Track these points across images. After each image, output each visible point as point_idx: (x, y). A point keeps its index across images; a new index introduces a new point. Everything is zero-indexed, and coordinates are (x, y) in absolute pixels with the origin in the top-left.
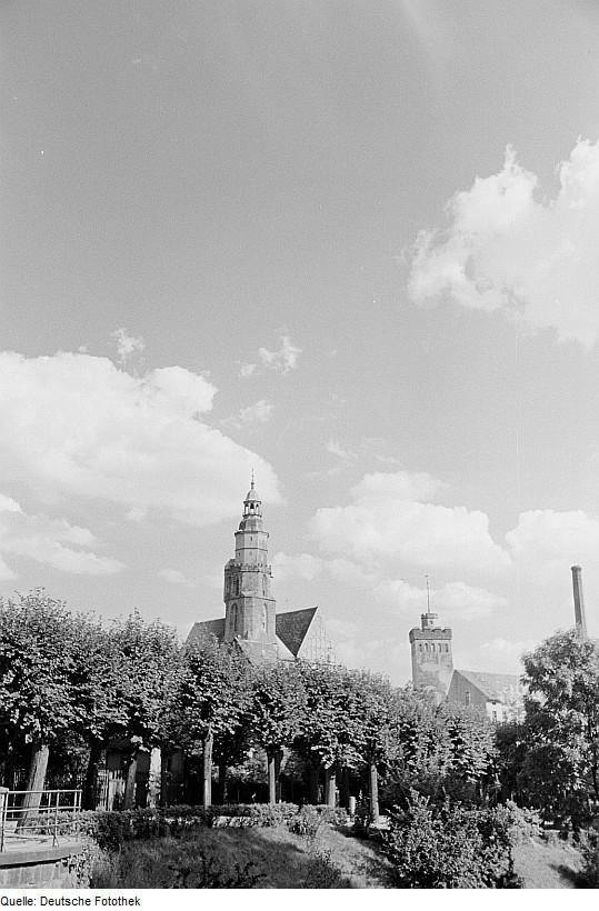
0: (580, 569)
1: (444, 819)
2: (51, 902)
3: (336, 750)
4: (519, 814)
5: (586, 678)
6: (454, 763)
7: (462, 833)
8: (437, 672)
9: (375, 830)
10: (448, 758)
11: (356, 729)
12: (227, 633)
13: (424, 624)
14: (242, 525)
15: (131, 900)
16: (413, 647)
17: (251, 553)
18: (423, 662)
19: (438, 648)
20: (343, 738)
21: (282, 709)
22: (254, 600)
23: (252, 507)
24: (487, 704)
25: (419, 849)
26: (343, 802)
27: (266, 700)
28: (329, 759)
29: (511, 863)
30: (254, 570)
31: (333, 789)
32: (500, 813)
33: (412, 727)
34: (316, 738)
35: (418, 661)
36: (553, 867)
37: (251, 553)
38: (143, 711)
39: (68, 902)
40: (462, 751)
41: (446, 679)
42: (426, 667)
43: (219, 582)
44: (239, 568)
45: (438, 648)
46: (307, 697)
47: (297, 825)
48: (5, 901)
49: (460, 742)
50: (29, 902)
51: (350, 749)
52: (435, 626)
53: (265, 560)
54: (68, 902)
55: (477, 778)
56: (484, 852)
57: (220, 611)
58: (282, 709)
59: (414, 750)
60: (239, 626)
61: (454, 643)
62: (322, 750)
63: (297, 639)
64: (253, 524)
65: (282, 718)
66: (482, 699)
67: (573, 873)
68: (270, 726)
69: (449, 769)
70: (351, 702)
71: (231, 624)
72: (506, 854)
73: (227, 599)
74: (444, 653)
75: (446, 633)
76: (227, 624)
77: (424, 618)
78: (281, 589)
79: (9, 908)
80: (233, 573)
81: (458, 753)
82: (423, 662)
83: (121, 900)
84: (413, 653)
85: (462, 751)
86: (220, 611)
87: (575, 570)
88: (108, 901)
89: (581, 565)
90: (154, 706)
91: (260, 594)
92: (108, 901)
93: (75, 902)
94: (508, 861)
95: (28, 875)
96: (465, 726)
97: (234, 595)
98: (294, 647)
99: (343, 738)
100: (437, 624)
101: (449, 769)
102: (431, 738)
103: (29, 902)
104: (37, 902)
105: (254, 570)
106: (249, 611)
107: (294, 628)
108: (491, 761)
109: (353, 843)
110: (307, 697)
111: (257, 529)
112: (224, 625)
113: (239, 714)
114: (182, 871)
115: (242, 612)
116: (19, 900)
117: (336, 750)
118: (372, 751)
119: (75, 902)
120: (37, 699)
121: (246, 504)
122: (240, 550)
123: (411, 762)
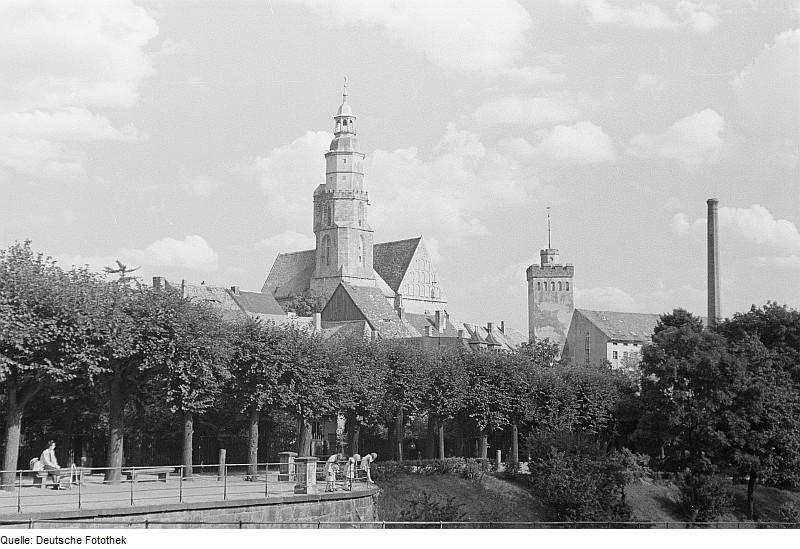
0: (717, 202)
1: (575, 468)
2: (46, 541)
3: (488, 417)
4: (633, 458)
5: (688, 366)
6: (579, 419)
7: (588, 476)
8: (556, 312)
9: (521, 475)
10: (574, 416)
11: (504, 399)
12: (318, 267)
13: (544, 260)
14: (334, 145)
15: (118, 539)
16: (531, 286)
17: (344, 178)
18: (540, 301)
20: (494, 407)
22: (349, 230)
23: (345, 123)
25: (557, 487)
26: (492, 455)
27: (438, 383)
29: (624, 496)
30: (348, 196)
31: (486, 446)
32: (615, 458)
34: (471, 409)
35: (536, 301)
36: (655, 498)
37: (344, 178)
38: (364, 398)
39: (61, 541)
40: (586, 409)
41: (565, 319)
42: (544, 307)
43: (305, 210)
46: (468, 378)
48: (4, 540)
49: (585, 401)
50: (26, 541)
51: (499, 416)
52: (556, 262)
54: (61, 541)
55: (597, 430)
56: (604, 489)
58: (451, 389)
59: (547, 412)
61: (575, 281)
63: (397, 273)
64: (346, 143)
65: (451, 396)
66: (603, 338)
67: (672, 503)
69: (575, 425)
72: (620, 490)
73: (318, 229)
74: (564, 291)
75: (568, 270)
76: (318, 256)
77: (544, 254)
79: (8, 546)
80: (324, 200)
81: (582, 411)
82: (540, 301)
83: (109, 540)
84: (530, 291)
85: (586, 409)
87: (711, 203)
88: (98, 541)
91: (356, 224)
92: (98, 541)
93: (68, 541)
94: (621, 495)
101: (575, 425)
103: (26, 541)
104: (34, 541)
105: (348, 196)
106: (342, 243)
107: (393, 259)
108: (611, 416)
110: (468, 378)
111: (351, 149)
114: (412, 502)
115: (336, 245)
116: (17, 540)
117: (488, 417)
118: (516, 416)
119: (68, 541)
120: (311, 397)
121: (338, 120)
122: (331, 174)
123: (544, 421)
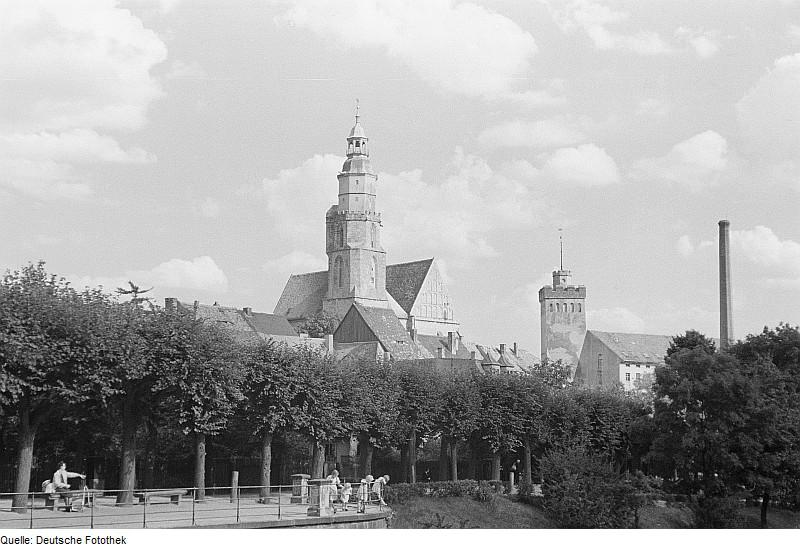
0: (728, 224)
2: (46, 541)
13: (556, 282)
14: (347, 166)
15: (118, 539)
16: (543, 307)
17: (357, 199)
18: (553, 323)
19: (569, 306)
21: (465, 411)
22: (361, 252)
23: (358, 145)
24: (621, 365)
27: (451, 405)
28: (496, 446)
30: (361, 218)
33: (559, 415)
37: (357, 199)
38: (377, 420)
39: (61, 541)
40: (599, 431)
41: (578, 340)
42: (557, 328)
44: (344, 216)
45: (569, 306)
47: (478, 495)
48: (4, 540)
49: (598, 423)
50: (26, 541)
51: (512, 438)
53: (373, 204)
54: (61, 541)
57: (322, 264)
58: (465, 411)
59: (560, 434)
60: (345, 281)
61: (587, 302)
62: (490, 439)
63: (410, 294)
64: (359, 165)
65: (464, 418)
68: (456, 424)
70: (514, 401)
71: (335, 279)
72: (633, 512)
73: (330, 250)
74: (576, 312)
75: (580, 291)
77: (556, 275)
78: (389, 240)
80: (336, 221)
82: (553, 323)
83: (109, 540)
85: (599, 431)
86: (322, 264)
87: (723, 225)
88: (98, 541)
89: (731, 222)
90: (386, 417)
91: (368, 246)
92: (98, 541)
93: (68, 541)
95: (375, 524)
96: (604, 410)
97: (338, 246)
98: (407, 303)
99: (507, 429)
100: (569, 282)
102: (575, 423)
103: (26, 541)
104: (34, 541)
105: (361, 218)
107: (406, 280)
109: (520, 507)
111: (364, 171)
112: (327, 280)
113: (435, 418)
115: (348, 266)
116: (17, 540)
117: (501, 439)
119: (68, 541)
120: (323, 419)
122: (344, 195)
